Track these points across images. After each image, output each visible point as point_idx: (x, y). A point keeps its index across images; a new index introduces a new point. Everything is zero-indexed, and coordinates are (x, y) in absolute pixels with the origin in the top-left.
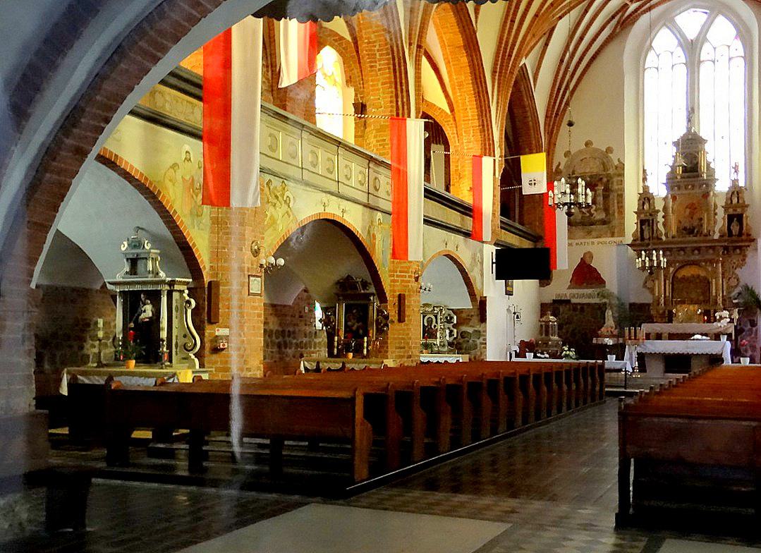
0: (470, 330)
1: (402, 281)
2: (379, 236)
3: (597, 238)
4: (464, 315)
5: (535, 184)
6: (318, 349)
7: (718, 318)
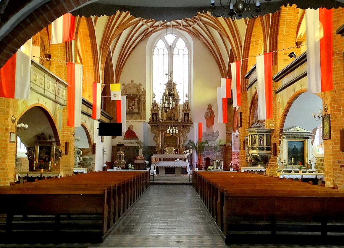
0: (88, 157)
1: (68, 136)
2: (58, 115)
3: (135, 119)
4: (85, 151)
5: (116, 96)
6: (17, 167)
7: (185, 153)
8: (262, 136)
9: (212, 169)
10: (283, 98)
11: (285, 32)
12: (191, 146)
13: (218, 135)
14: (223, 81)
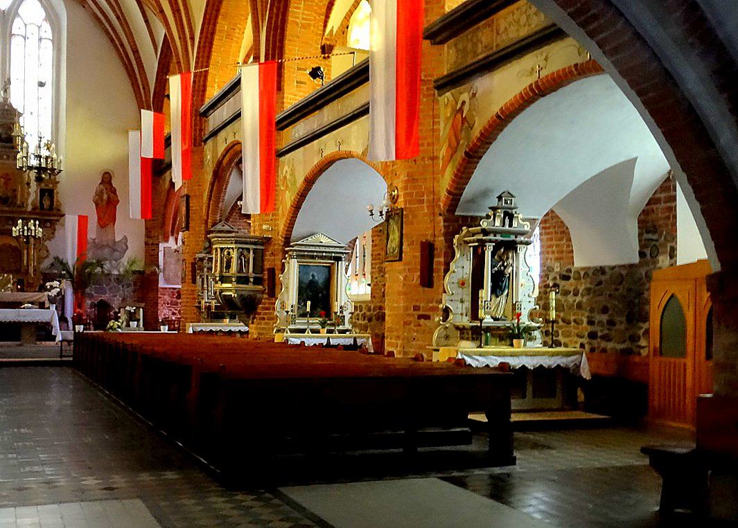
7: (48, 287)
8: (245, 253)
9: (119, 327)
10: (295, 167)
11: (303, 19)
12: (58, 270)
13: (125, 248)
14: (148, 116)
